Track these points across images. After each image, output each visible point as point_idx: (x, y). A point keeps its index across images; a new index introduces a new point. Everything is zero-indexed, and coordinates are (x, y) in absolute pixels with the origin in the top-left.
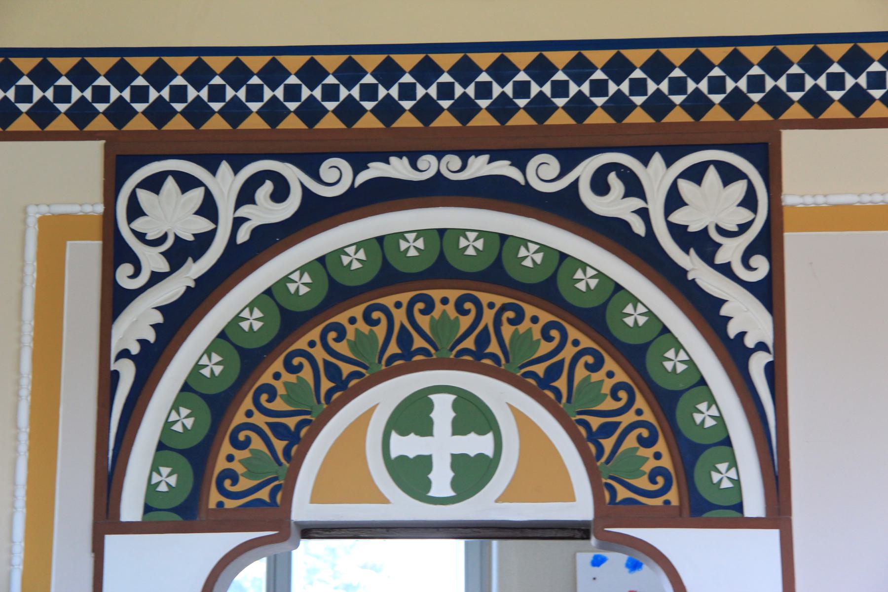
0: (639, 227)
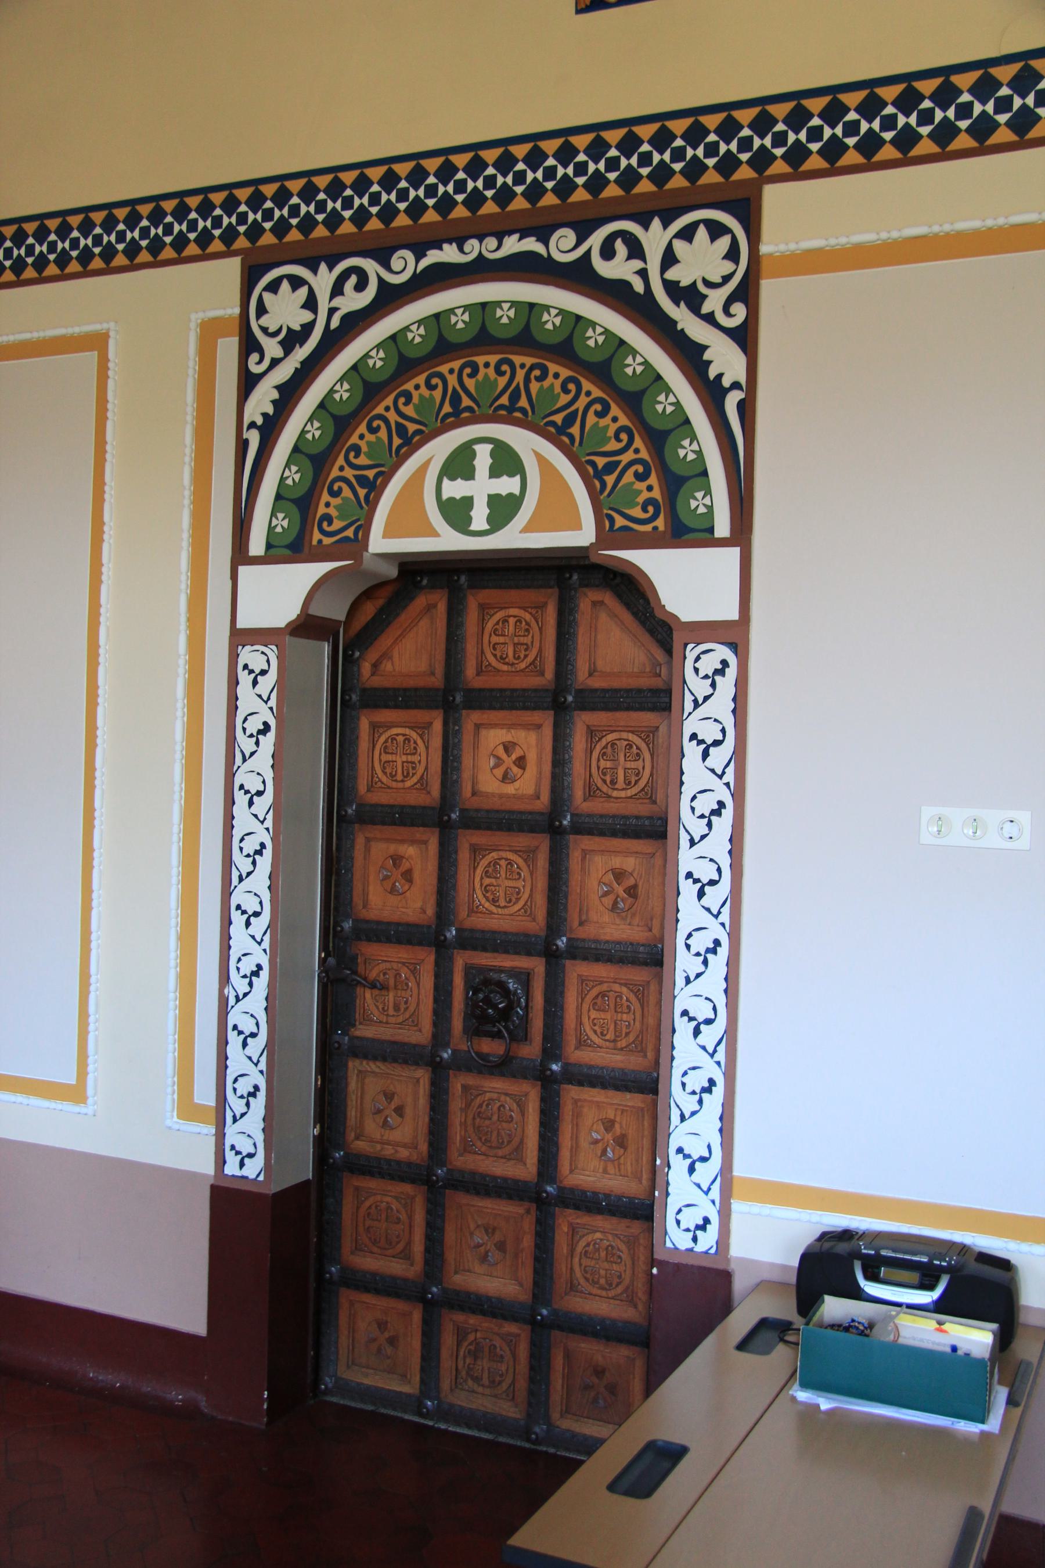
0: (639, 287)
